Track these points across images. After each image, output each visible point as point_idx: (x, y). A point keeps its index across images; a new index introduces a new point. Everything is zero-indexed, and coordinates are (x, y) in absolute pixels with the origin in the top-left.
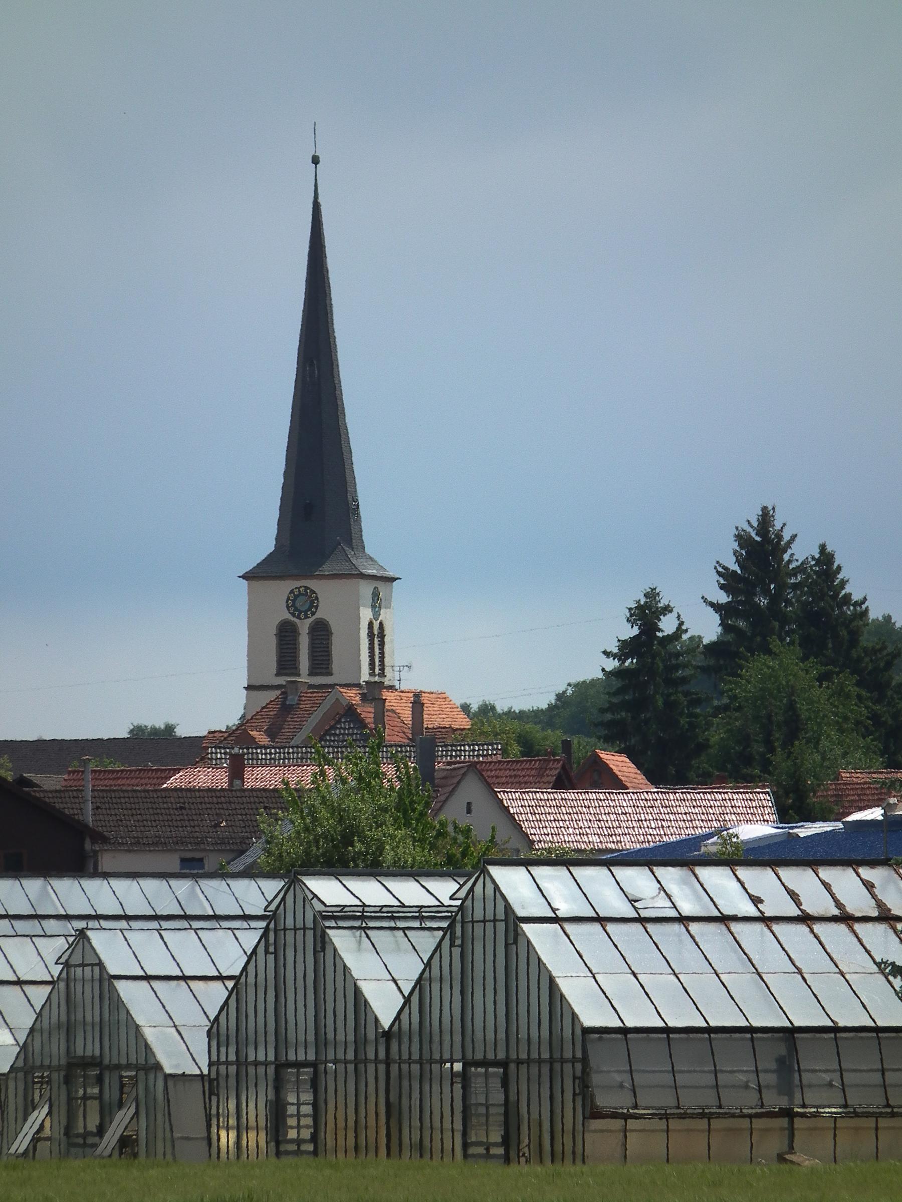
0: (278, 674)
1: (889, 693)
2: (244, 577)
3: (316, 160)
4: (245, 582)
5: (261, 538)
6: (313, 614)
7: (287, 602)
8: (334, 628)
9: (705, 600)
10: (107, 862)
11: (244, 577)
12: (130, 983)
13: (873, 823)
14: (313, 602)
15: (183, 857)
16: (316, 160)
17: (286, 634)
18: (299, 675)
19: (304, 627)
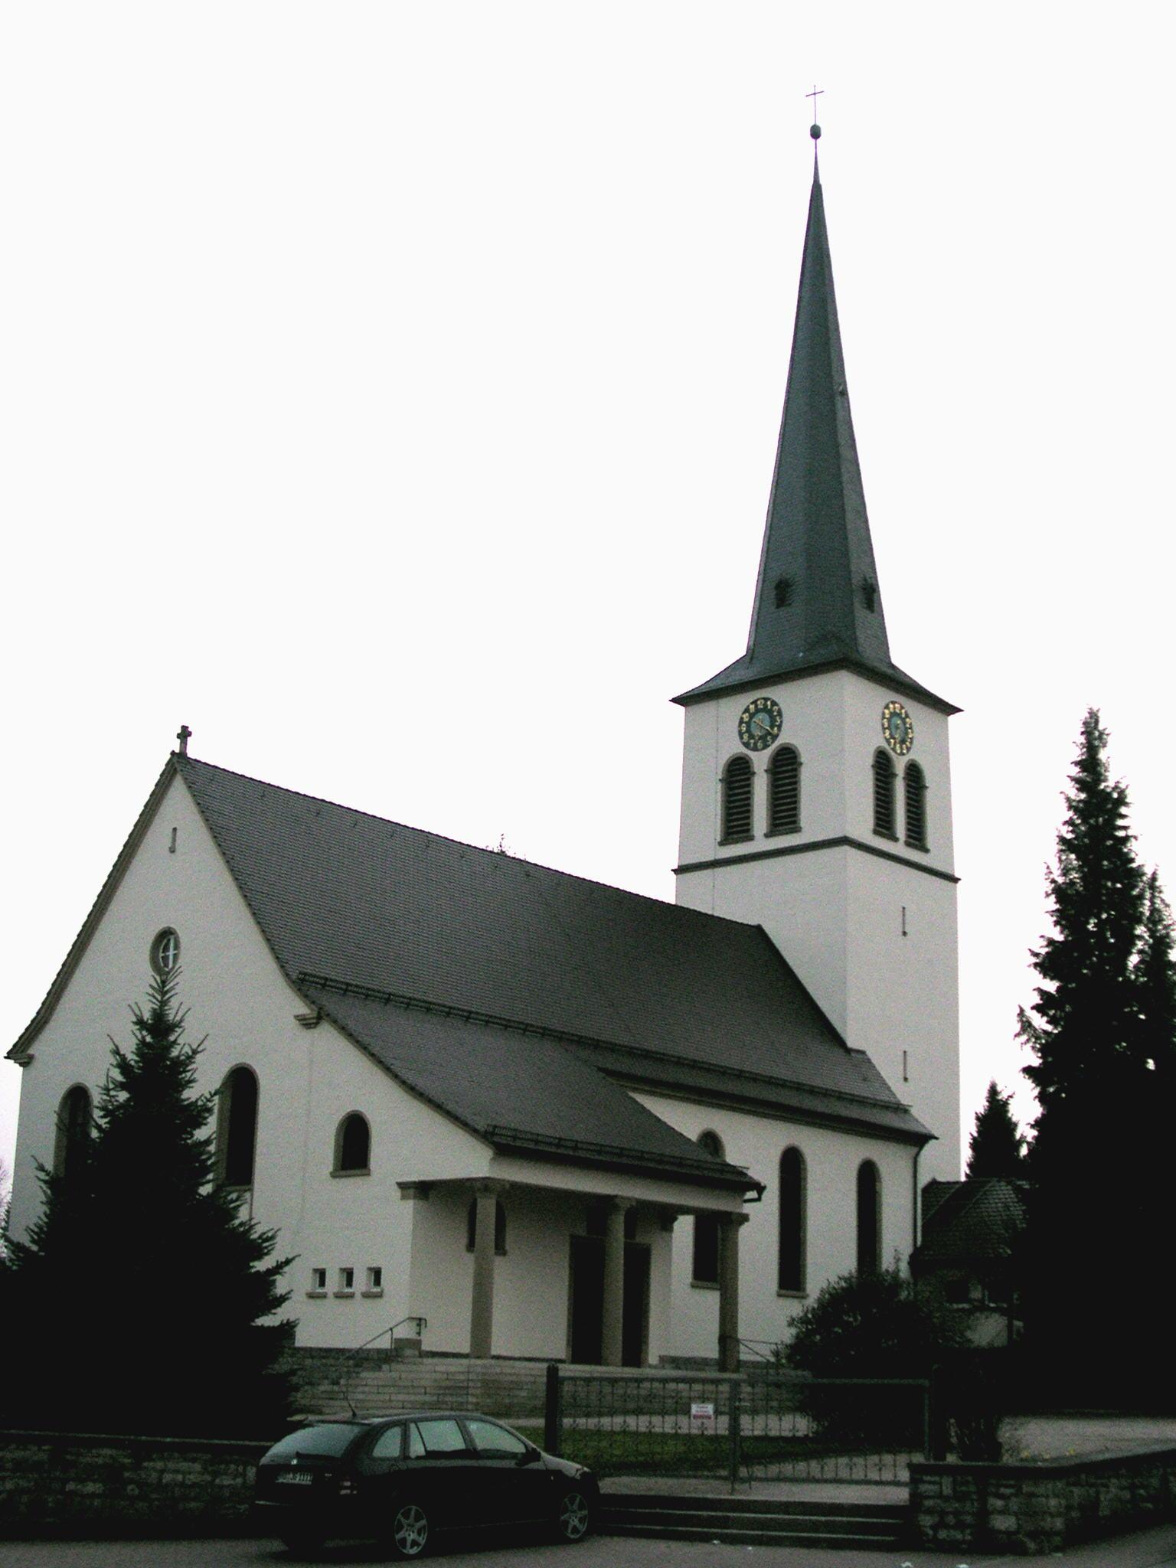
0: (722, 844)
1: (1141, 885)
2: (675, 700)
3: (815, 133)
4: (680, 710)
5: (725, 636)
6: (775, 737)
7: (741, 738)
8: (804, 758)
9: (1093, 737)
10: (508, 1186)
11: (675, 700)
12: (920, 1170)
13: (509, 1470)
14: (773, 713)
15: (493, 1251)
16: (815, 133)
17: (737, 773)
18: (751, 838)
19: (761, 761)
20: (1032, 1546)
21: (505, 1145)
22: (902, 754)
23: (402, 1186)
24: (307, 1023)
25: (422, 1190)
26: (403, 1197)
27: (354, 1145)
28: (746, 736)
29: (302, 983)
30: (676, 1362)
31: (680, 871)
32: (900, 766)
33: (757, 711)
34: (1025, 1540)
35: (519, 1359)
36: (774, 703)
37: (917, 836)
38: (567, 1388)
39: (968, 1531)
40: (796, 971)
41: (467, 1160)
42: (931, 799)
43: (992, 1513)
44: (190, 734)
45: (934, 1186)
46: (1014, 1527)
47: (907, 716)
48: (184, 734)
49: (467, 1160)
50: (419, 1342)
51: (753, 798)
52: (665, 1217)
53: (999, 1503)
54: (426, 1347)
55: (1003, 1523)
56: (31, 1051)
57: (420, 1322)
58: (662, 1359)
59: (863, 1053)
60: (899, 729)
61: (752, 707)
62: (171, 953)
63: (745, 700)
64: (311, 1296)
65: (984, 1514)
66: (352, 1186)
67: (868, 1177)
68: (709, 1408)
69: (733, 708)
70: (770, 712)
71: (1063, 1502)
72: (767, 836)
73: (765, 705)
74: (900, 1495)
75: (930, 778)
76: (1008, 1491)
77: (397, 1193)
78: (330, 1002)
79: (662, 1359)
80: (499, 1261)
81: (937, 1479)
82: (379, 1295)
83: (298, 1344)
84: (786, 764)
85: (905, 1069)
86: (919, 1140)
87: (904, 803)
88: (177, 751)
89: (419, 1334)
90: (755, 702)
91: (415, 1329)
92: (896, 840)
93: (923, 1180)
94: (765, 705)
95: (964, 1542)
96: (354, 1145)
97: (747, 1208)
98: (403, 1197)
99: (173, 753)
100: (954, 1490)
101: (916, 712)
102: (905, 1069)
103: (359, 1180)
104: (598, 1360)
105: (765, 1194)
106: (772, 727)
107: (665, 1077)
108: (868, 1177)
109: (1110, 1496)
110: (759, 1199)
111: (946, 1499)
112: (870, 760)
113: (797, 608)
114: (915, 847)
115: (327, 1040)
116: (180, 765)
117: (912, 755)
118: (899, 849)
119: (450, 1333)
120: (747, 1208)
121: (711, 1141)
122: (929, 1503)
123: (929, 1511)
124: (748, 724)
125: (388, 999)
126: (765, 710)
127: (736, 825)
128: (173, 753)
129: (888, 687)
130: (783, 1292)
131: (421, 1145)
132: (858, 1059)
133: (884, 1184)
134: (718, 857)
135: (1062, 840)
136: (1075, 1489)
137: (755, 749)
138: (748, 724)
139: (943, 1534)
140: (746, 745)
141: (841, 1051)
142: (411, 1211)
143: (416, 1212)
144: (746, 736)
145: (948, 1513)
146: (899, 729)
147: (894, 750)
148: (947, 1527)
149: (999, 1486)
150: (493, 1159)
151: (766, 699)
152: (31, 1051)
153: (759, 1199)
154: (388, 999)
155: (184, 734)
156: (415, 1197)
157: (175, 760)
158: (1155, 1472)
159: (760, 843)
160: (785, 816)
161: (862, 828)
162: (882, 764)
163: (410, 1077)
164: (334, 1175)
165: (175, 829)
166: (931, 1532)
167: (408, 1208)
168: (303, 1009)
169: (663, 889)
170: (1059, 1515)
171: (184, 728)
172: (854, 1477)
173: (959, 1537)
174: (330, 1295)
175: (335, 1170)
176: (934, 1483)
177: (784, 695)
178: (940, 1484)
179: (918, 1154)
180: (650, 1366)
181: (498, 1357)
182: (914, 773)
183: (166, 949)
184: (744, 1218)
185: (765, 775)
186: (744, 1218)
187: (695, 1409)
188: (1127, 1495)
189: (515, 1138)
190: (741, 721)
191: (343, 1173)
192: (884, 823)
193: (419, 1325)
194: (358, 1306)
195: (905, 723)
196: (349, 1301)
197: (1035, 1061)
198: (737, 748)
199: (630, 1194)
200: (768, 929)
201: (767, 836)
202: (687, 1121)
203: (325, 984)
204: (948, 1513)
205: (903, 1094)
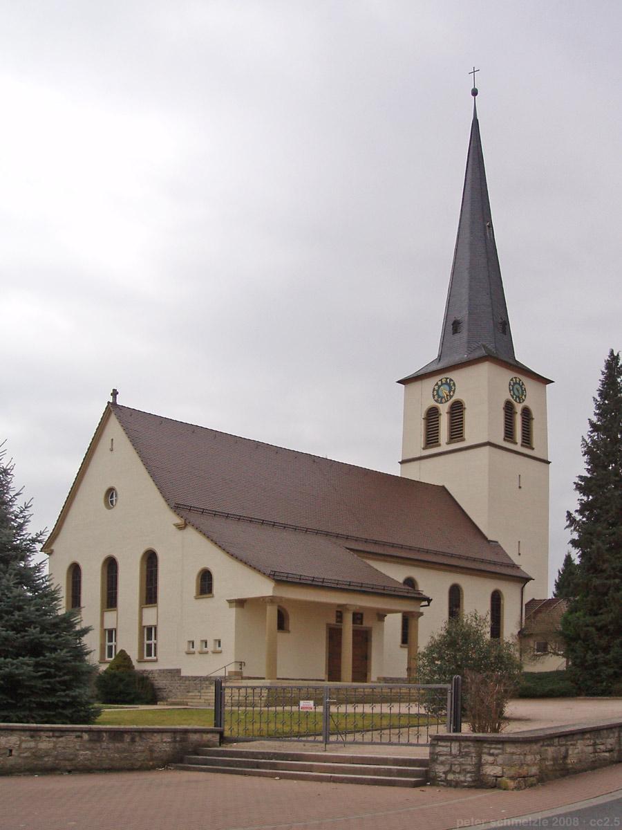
0: (424, 449)
2: (398, 382)
3: (475, 93)
5: (427, 352)
7: (434, 398)
11: (398, 382)
14: (451, 385)
16: (475, 93)
17: (432, 416)
18: (440, 445)
19: (444, 409)
20: (512, 784)
21: (280, 580)
22: (520, 402)
23: (230, 602)
24: (181, 528)
25: (240, 603)
26: (230, 607)
27: (205, 583)
28: (436, 397)
29: (177, 508)
30: (386, 680)
31: (402, 463)
32: (519, 408)
33: (442, 384)
34: (507, 781)
35: (299, 680)
36: (451, 380)
37: (527, 441)
38: (227, 691)
39: (469, 775)
40: (462, 506)
41: (263, 588)
42: (535, 426)
43: (485, 764)
44: (118, 393)
45: (533, 602)
46: (500, 773)
47: (523, 384)
48: (115, 393)
49: (263, 588)
50: (241, 673)
51: (442, 426)
52: (381, 615)
53: (491, 759)
54: (245, 675)
55: (491, 771)
56: (52, 548)
57: (241, 664)
58: (378, 678)
59: (497, 542)
60: (518, 391)
61: (440, 383)
62: (114, 499)
63: (436, 380)
64: (188, 653)
65: (479, 765)
66: (205, 602)
67: (496, 599)
68: (311, 703)
69: (430, 384)
70: (449, 385)
71: (538, 757)
72: (448, 444)
73: (446, 381)
74: (423, 753)
75: (535, 414)
76: (496, 752)
77: (227, 604)
78: (193, 517)
79: (378, 678)
80: (281, 636)
81: (449, 744)
82: (221, 652)
83: (182, 675)
84: (457, 410)
85: (519, 550)
86: (525, 580)
87: (520, 427)
88: (111, 401)
89: (241, 669)
90: (441, 380)
91: (240, 667)
92: (516, 443)
93: (527, 599)
94: (446, 381)
95: (465, 782)
96: (205, 583)
97: (422, 609)
98: (230, 607)
99: (109, 403)
100: (460, 750)
101: (529, 384)
102: (519, 550)
103: (208, 600)
104: (339, 679)
105: (431, 604)
106: (450, 392)
107: (395, 554)
108: (496, 599)
109: (576, 751)
110: (428, 605)
111: (455, 756)
112: (502, 405)
113: (464, 334)
114: (527, 447)
115: (191, 534)
116: (113, 408)
117: (525, 403)
118: (518, 448)
119: (257, 666)
120: (422, 609)
121: (410, 582)
122: (442, 758)
123: (442, 763)
124: (437, 391)
125: (227, 516)
126: (446, 383)
127: (431, 438)
128: (109, 403)
129: (512, 370)
130: (403, 645)
131: (236, 581)
132: (494, 545)
133: (505, 601)
134: (423, 455)
135: (593, 425)
136: (549, 748)
137: (441, 403)
138: (437, 391)
139: (450, 777)
140: (436, 401)
141: (485, 542)
142: (234, 613)
143: (236, 611)
144: (436, 397)
145: (455, 764)
146: (518, 391)
147: (516, 400)
148: (454, 772)
149: (491, 748)
150: (274, 588)
151: (447, 379)
152: (52, 548)
153: (428, 605)
154: (227, 516)
155: (115, 393)
156: (236, 607)
157: (110, 405)
158: (611, 735)
159: (444, 447)
160: (457, 432)
161: (499, 439)
162: (509, 408)
163: (232, 550)
164: (196, 598)
165: (112, 440)
166: (444, 776)
167: (232, 612)
168: (179, 521)
169: (396, 470)
170: (534, 764)
171: (114, 390)
172: (383, 741)
173: (462, 778)
174: (196, 652)
175: (197, 595)
176: (446, 746)
177: (454, 376)
178: (451, 747)
179: (524, 586)
180: (372, 682)
181: (278, 679)
182: (526, 413)
183: (112, 497)
184: (422, 614)
185: (446, 415)
186: (422, 614)
187: (302, 703)
188: (590, 749)
189: (313, 581)
190: (434, 390)
191: (200, 596)
192: (509, 435)
193: (241, 665)
194: (211, 656)
195: (522, 388)
196: (220, 654)
197: (576, 536)
198: (431, 403)
199: (352, 603)
200: (446, 487)
201: (448, 444)
202: (397, 574)
203: (190, 509)
204: (455, 764)
205: (516, 560)
